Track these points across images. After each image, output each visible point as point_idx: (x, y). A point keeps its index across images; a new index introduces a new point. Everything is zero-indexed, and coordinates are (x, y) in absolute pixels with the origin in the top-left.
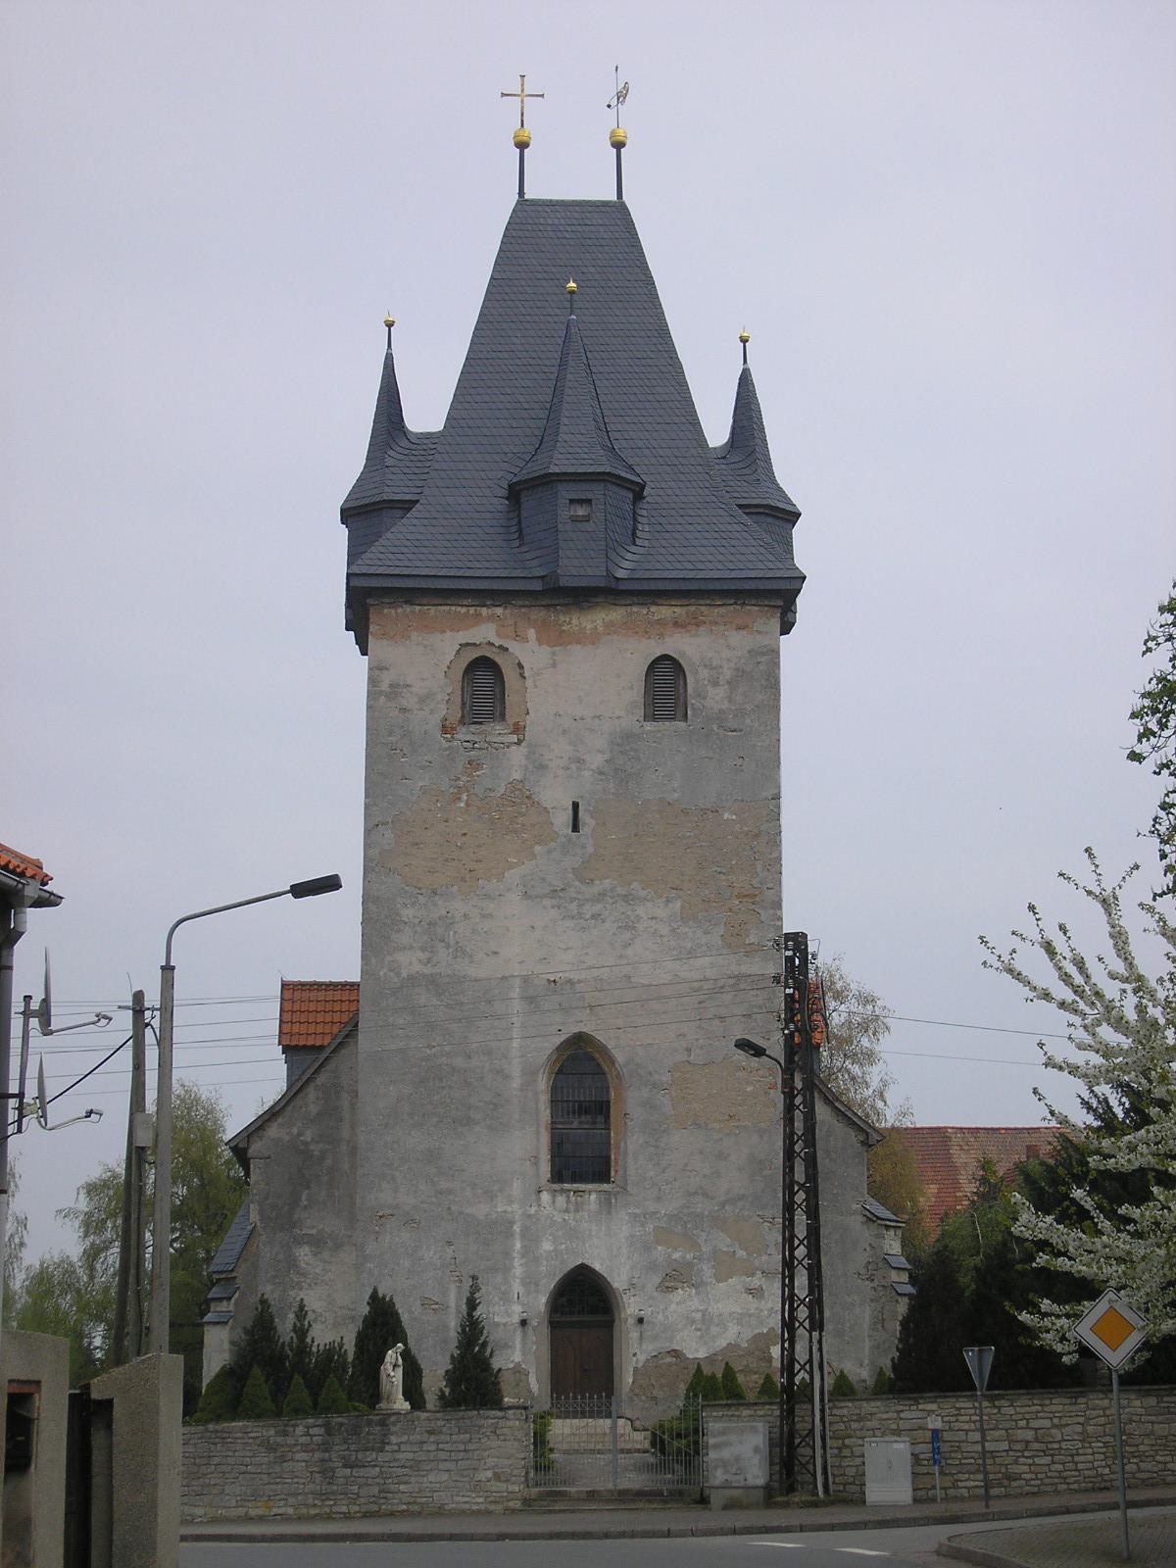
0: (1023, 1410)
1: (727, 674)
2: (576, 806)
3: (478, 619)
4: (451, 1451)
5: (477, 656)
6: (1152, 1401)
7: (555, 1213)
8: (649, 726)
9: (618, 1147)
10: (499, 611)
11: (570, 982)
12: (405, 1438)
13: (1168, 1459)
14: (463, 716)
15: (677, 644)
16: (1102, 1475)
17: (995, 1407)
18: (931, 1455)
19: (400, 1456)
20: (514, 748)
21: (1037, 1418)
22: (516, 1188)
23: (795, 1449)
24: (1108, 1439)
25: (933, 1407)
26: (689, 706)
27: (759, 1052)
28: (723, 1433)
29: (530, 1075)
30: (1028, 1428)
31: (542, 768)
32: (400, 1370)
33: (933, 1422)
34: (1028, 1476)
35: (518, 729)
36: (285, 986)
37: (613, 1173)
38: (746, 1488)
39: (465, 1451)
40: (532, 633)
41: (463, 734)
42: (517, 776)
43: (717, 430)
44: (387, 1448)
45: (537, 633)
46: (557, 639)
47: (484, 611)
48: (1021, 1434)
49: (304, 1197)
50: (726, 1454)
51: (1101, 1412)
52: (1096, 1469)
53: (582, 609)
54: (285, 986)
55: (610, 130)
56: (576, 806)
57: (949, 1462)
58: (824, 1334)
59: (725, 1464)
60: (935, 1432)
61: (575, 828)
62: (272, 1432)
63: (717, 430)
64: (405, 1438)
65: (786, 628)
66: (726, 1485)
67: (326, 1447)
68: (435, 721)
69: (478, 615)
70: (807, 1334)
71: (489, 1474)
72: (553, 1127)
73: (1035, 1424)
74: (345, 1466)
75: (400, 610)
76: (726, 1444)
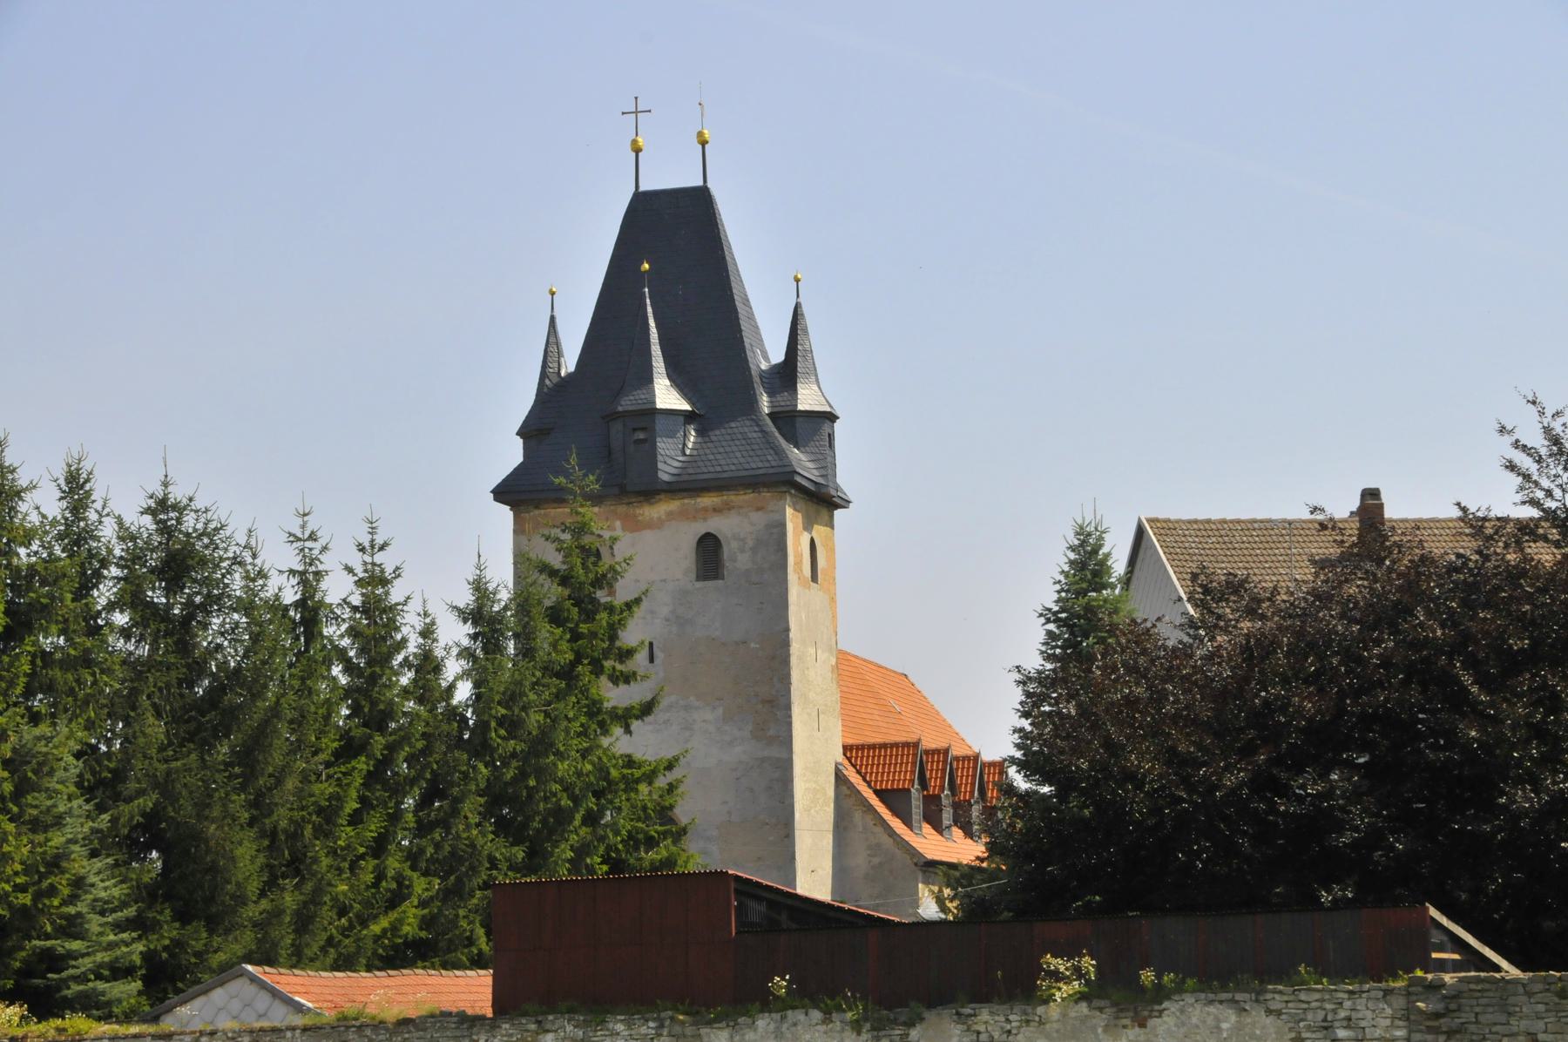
1: (750, 543)
2: (651, 644)
8: (699, 584)
15: (720, 525)
46: (634, 525)
53: (651, 504)
56: (651, 644)
61: (652, 660)
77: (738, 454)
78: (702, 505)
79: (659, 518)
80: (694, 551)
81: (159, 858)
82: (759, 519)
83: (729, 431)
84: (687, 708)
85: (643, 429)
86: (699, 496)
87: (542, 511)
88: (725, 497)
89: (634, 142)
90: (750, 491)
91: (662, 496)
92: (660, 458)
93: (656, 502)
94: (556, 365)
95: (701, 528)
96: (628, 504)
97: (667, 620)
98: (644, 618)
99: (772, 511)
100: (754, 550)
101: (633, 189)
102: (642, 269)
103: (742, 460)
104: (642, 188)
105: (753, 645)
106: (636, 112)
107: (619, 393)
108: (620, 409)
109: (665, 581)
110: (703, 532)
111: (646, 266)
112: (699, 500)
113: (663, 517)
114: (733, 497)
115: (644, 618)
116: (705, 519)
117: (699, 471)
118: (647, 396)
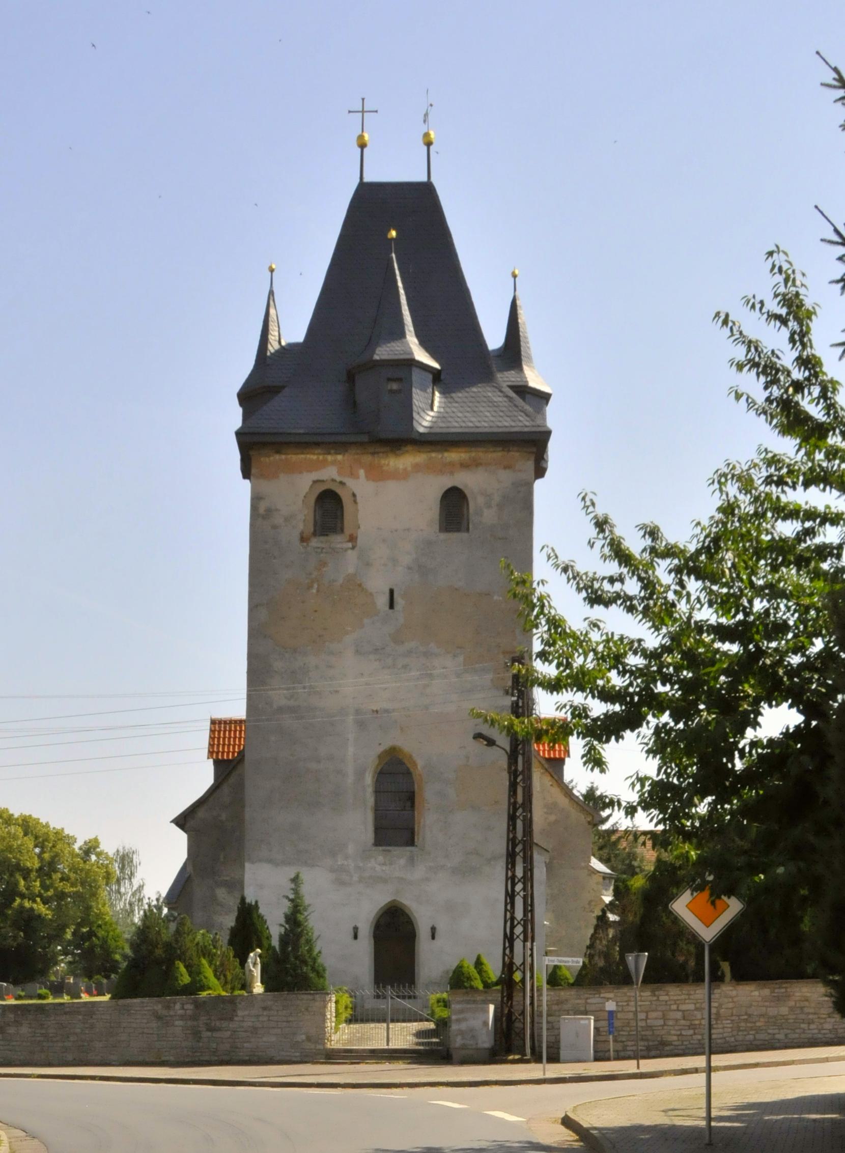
0: (675, 998)
1: (497, 499)
2: (392, 592)
3: (324, 464)
4: (278, 1022)
5: (323, 489)
6: (766, 992)
7: (377, 866)
8: (443, 536)
9: (419, 823)
10: (340, 457)
11: (387, 711)
12: (246, 1013)
13: (776, 1031)
14: (315, 531)
15: (466, 480)
16: (728, 1042)
17: (655, 995)
18: (607, 1028)
19: (245, 1024)
20: (350, 552)
21: (685, 1003)
22: (351, 849)
23: (513, 1023)
24: (733, 1018)
25: (611, 995)
26: (470, 522)
27: (491, 742)
28: (461, 1011)
29: (360, 774)
30: (678, 1010)
31: (368, 564)
32: (259, 967)
33: (611, 1006)
34: (676, 1043)
35: (353, 539)
36: (213, 722)
37: (416, 840)
38: (478, 1049)
39: (288, 1022)
40: (362, 472)
41: (315, 542)
42: (351, 570)
43: (494, 338)
44: (236, 1019)
45: (366, 472)
46: (377, 475)
47: (329, 458)
48: (672, 1015)
49: (222, 857)
50: (463, 1026)
51: (730, 1000)
52: (725, 1038)
53: (397, 455)
54: (213, 722)
55: (510, 273)
56: (392, 592)
57: (621, 1033)
58: (535, 944)
59: (461, 1033)
60: (611, 1013)
61: (392, 605)
62: (160, 1006)
63: (494, 338)
64: (246, 1013)
65: (540, 472)
66: (464, 1047)
67: (194, 1018)
68: (296, 535)
69: (325, 461)
70: (522, 943)
71: (304, 1037)
72: (376, 809)
73: (683, 1007)
74: (208, 1030)
75: (272, 458)
76: (465, 1019)
77: (488, 414)
78: (448, 460)
79: (405, 470)
80: (439, 503)
81: (693, 776)
82: (506, 477)
83: (473, 395)
84: (426, 654)
85: (399, 380)
86: (446, 451)
87: (283, 457)
88: (473, 454)
89: (361, 137)
90: (501, 449)
91: (409, 448)
92: (415, 408)
93: (402, 454)
94: (277, 334)
95: (447, 482)
96: (373, 454)
97: (409, 568)
98: (385, 565)
99: (520, 471)
100: (501, 507)
101: (358, 181)
102: (389, 236)
103: (492, 419)
104: (367, 179)
105: (496, 598)
106: (363, 112)
107: (371, 344)
108: (376, 357)
109: (408, 530)
110: (450, 485)
111: (393, 233)
112: (446, 454)
113: (409, 469)
114: (481, 454)
115: (385, 565)
116: (452, 473)
117: (449, 425)
118: (403, 348)
